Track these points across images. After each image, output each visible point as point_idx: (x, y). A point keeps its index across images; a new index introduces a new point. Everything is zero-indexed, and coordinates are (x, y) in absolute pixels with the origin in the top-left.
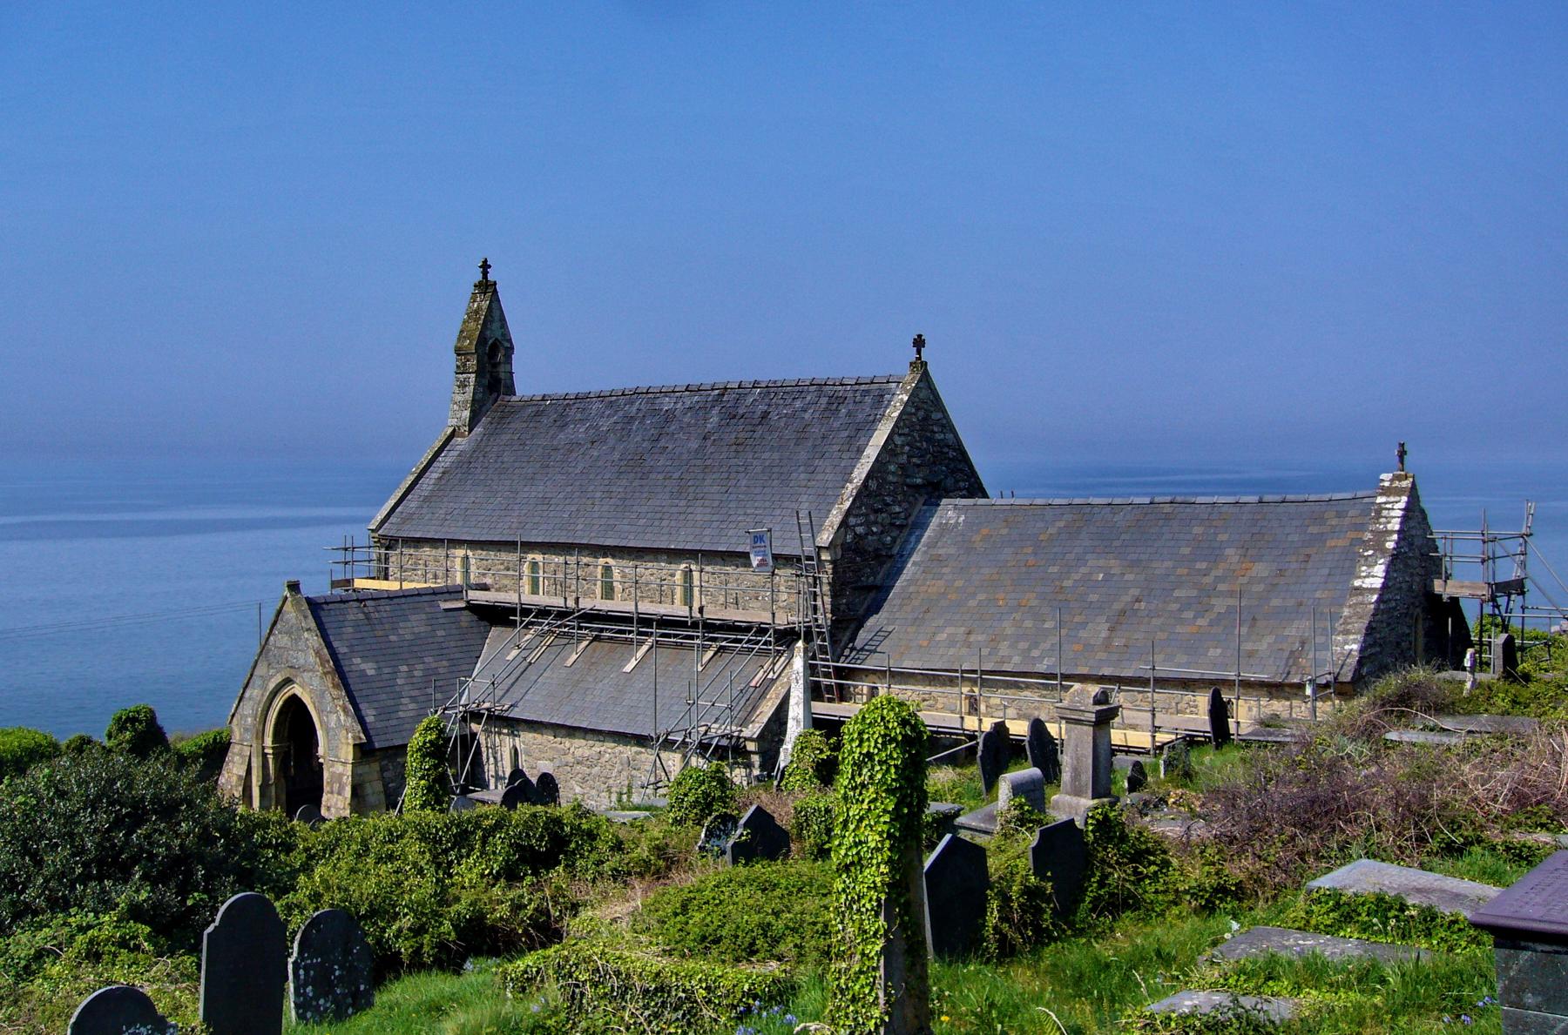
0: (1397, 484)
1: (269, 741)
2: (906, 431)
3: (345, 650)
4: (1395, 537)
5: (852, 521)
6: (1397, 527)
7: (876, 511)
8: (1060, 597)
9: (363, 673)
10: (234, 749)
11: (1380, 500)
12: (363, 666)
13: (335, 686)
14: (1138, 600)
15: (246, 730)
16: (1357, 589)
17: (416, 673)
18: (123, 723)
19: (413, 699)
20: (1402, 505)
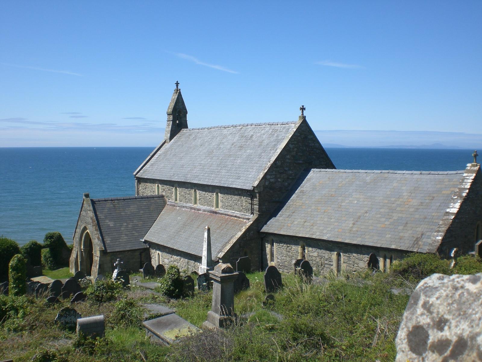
0: (473, 168)
1: (82, 246)
2: (296, 142)
3: (102, 217)
4: (467, 191)
5: (268, 177)
6: (469, 187)
7: (281, 173)
8: (339, 209)
9: (109, 226)
10: (74, 249)
11: (465, 175)
12: (109, 223)
13: (96, 230)
14: (366, 213)
15: (77, 242)
16: (447, 213)
17: (129, 226)
18: (50, 237)
19: (126, 235)
20: (473, 177)
